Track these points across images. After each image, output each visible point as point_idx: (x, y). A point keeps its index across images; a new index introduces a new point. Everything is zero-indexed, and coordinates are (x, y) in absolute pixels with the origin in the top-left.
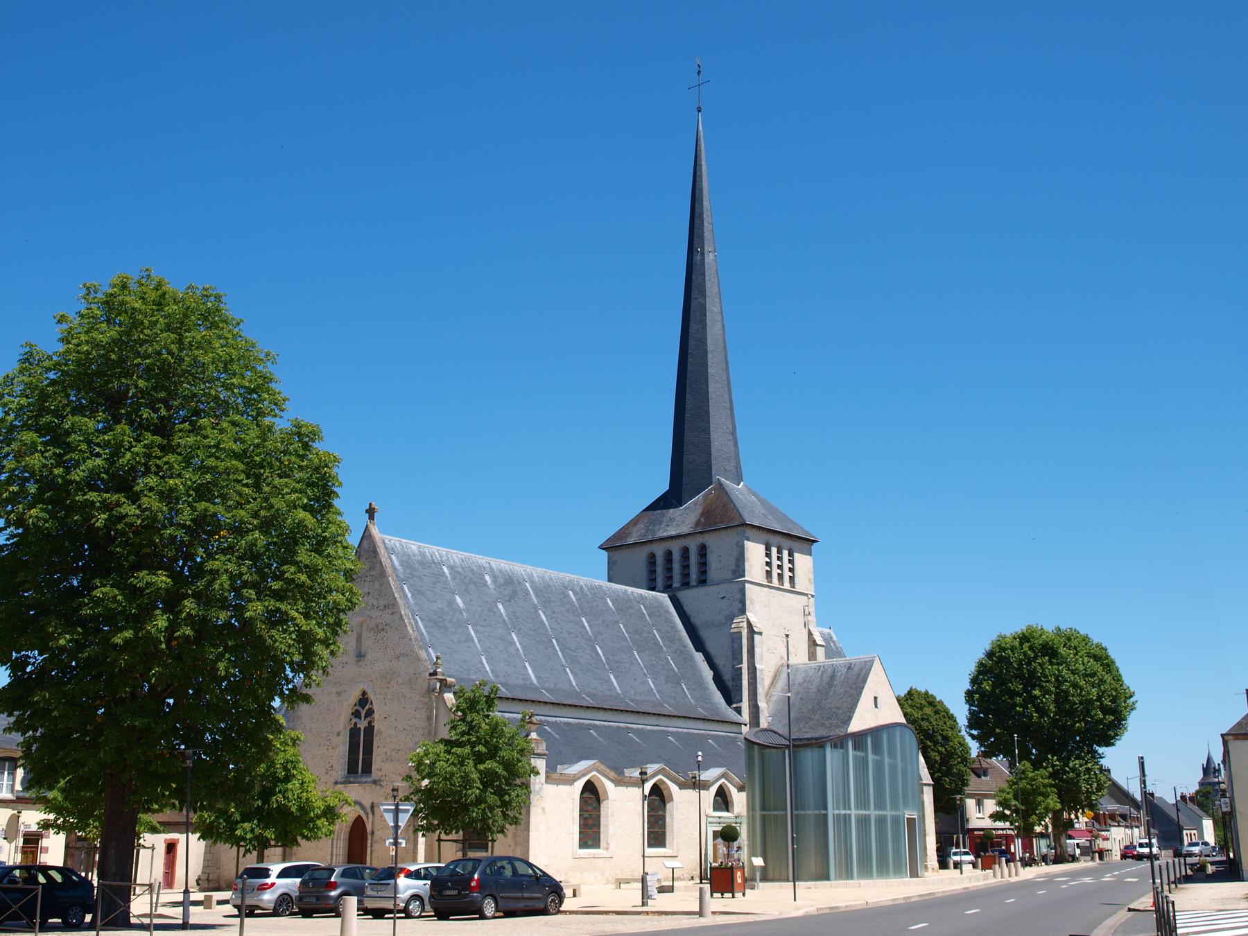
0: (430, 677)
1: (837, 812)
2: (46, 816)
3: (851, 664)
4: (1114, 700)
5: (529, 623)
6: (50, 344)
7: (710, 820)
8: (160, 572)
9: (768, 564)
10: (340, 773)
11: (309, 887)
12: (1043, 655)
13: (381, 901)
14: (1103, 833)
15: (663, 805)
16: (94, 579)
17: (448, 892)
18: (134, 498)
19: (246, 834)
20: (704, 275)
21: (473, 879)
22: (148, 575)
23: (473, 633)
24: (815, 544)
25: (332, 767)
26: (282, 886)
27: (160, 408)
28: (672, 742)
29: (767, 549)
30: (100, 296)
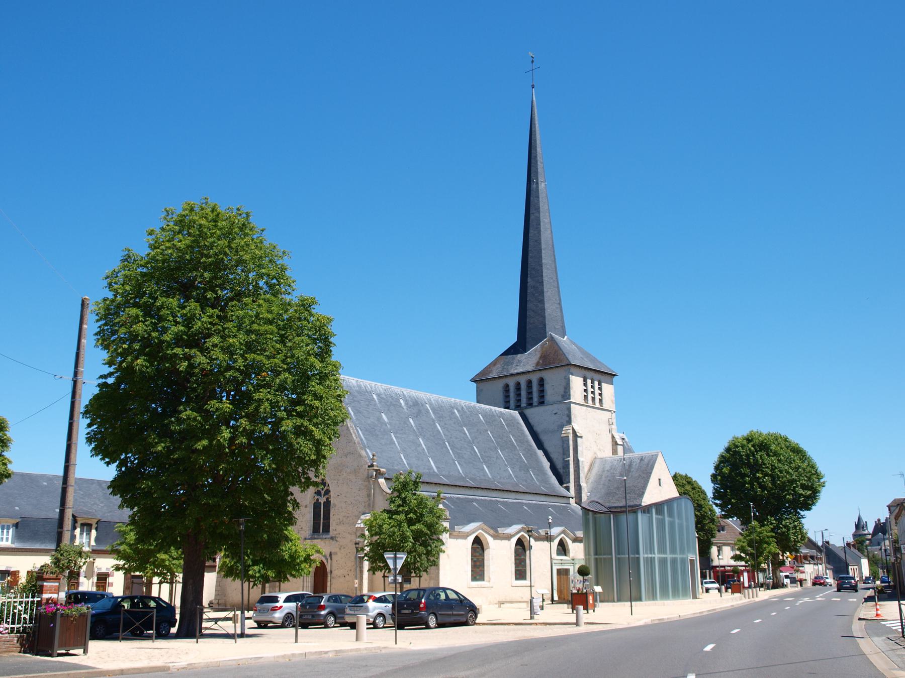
0: (368, 468)
1: (646, 556)
2: (117, 562)
3: (642, 457)
4: (809, 479)
5: (429, 431)
6: (142, 250)
7: (555, 561)
9: (585, 391)
10: (308, 532)
11: (306, 608)
14: (800, 568)
15: (524, 552)
16: (180, 407)
17: (405, 611)
18: (204, 350)
20: (538, 197)
21: (421, 602)
22: (217, 403)
24: (615, 377)
25: (302, 528)
27: (218, 290)
28: (525, 510)
30: (175, 218)
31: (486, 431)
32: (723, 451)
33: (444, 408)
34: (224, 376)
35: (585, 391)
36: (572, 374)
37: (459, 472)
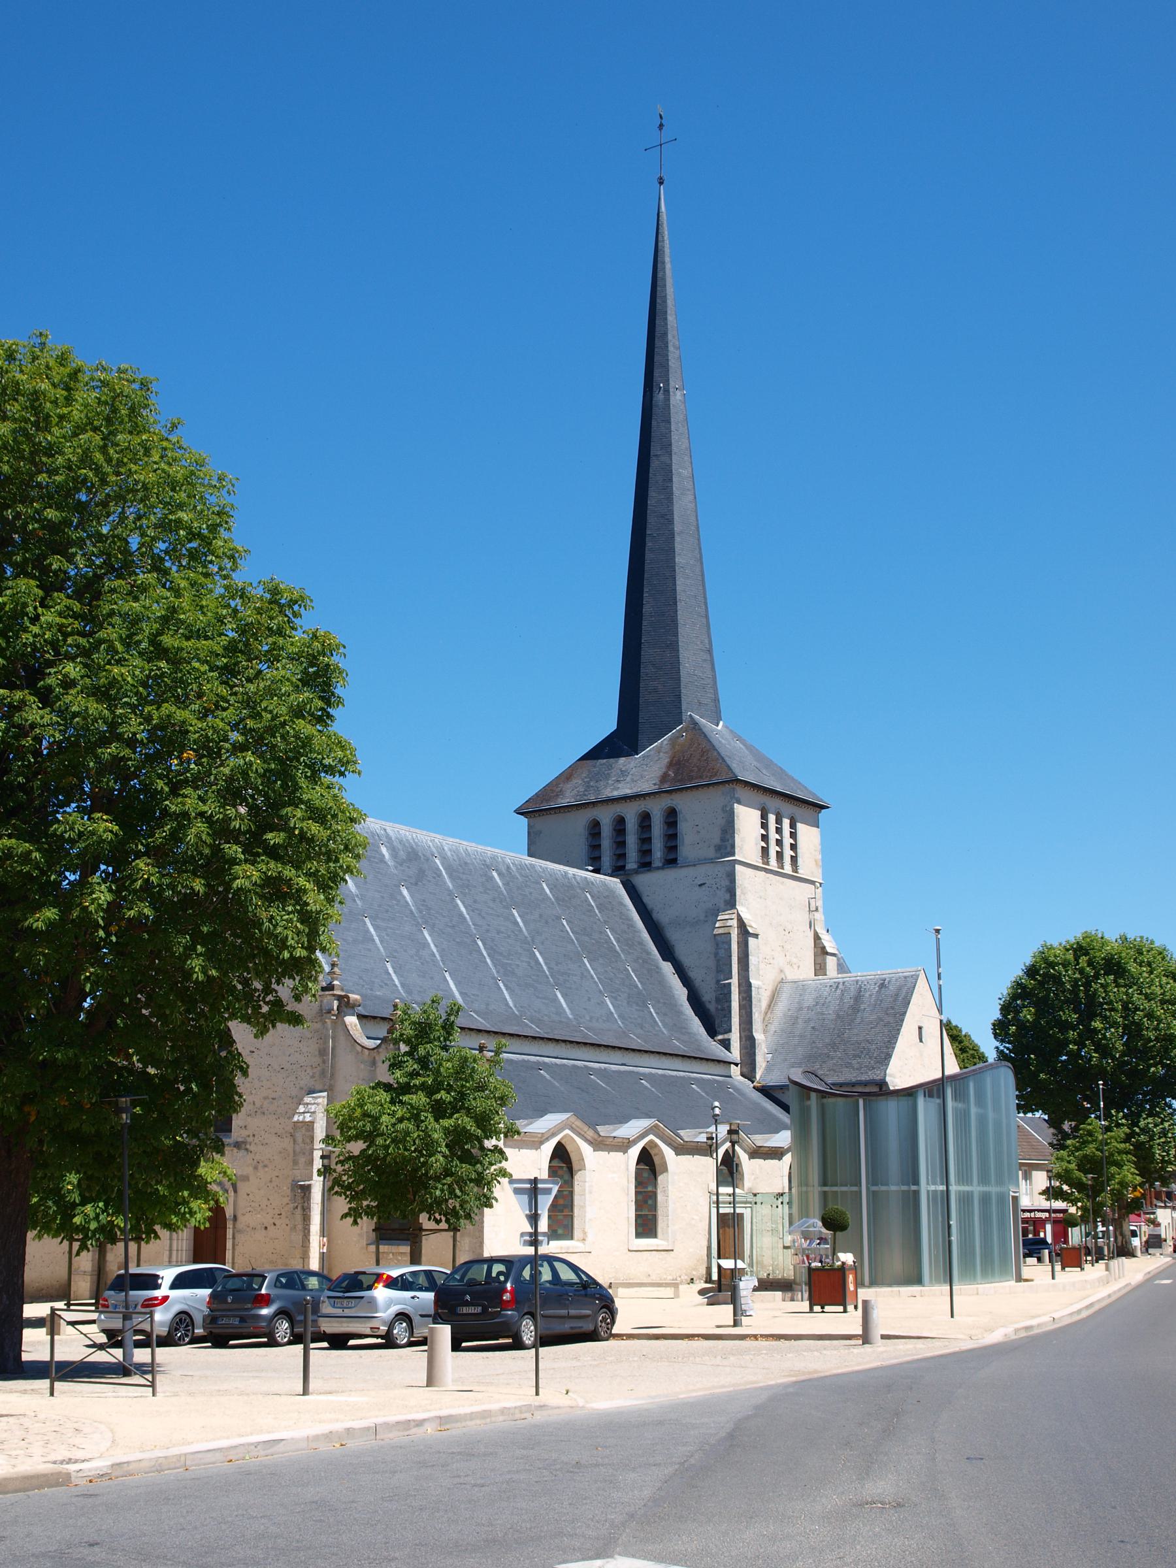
1: (932, 1188)
5: (444, 917)
8: (99, 815)
9: (765, 838)
11: (226, 1302)
12: (1107, 974)
13: (351, 1322)
15: (652, 1176)
19: (89, 1222)
20: (669, 422)
21: (505, 1290)
23: (372, 929)
24: (823, 811)
26: (177, 1301)
29: (762, 817)
31: (558, 918)
32: (1021, 973)
33: (471, 867)
34: (97, 757)
35: (765, 838)
36: (739, 803)
37: (507, 1004)
